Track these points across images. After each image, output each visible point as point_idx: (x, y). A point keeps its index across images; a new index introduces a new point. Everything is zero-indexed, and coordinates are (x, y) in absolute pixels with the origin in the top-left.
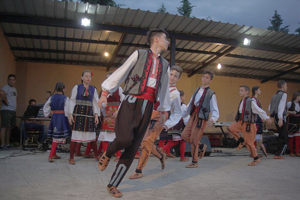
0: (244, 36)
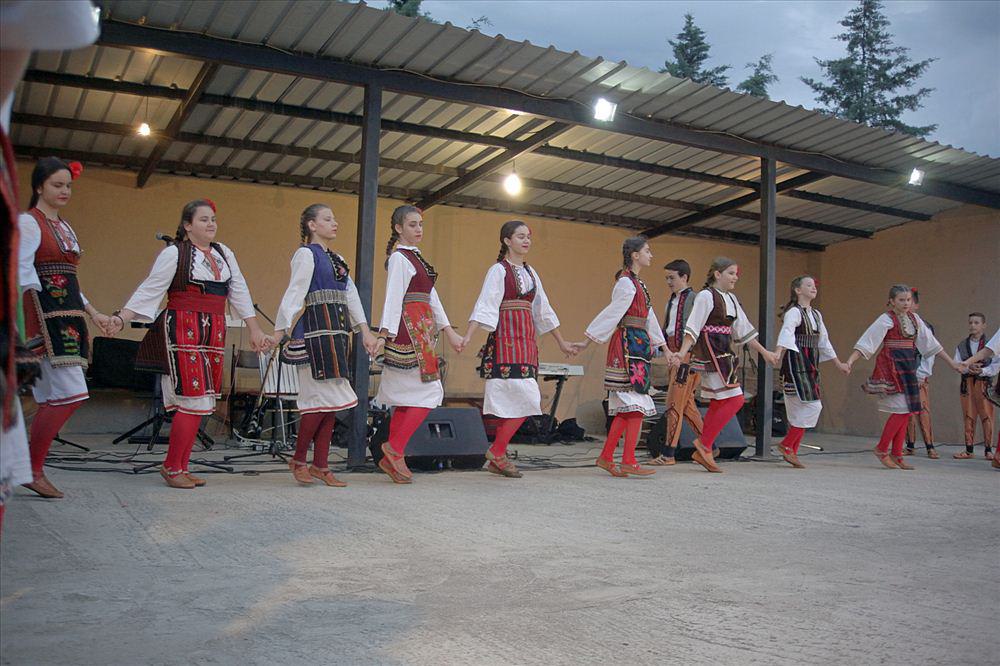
0: (596, 89)
